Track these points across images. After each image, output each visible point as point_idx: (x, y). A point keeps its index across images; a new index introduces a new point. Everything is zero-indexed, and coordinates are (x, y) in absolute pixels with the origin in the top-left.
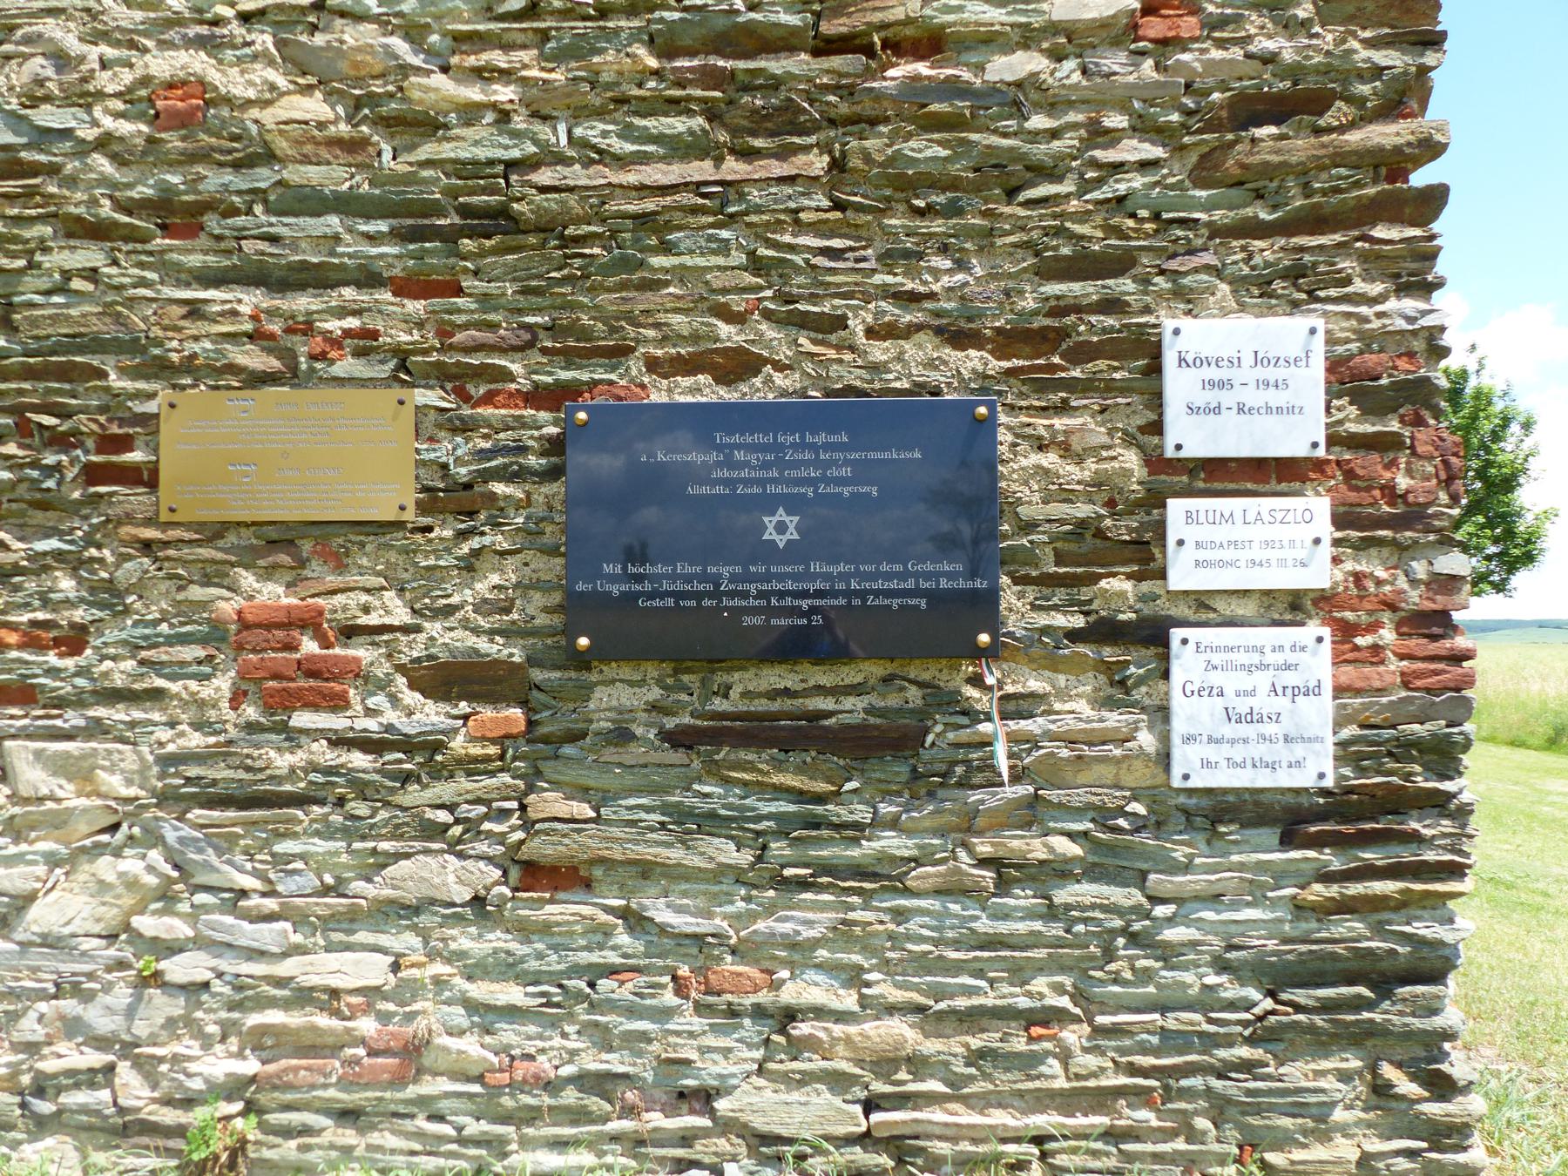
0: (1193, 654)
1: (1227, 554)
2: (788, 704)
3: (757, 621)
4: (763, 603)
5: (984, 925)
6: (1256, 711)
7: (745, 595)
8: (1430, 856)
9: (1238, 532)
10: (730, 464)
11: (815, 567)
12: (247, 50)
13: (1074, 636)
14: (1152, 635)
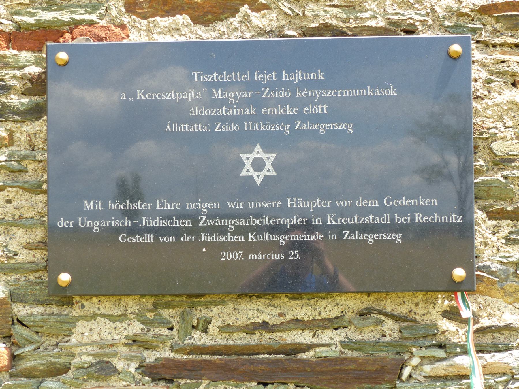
3: (235, 256)
7: (223, 231)
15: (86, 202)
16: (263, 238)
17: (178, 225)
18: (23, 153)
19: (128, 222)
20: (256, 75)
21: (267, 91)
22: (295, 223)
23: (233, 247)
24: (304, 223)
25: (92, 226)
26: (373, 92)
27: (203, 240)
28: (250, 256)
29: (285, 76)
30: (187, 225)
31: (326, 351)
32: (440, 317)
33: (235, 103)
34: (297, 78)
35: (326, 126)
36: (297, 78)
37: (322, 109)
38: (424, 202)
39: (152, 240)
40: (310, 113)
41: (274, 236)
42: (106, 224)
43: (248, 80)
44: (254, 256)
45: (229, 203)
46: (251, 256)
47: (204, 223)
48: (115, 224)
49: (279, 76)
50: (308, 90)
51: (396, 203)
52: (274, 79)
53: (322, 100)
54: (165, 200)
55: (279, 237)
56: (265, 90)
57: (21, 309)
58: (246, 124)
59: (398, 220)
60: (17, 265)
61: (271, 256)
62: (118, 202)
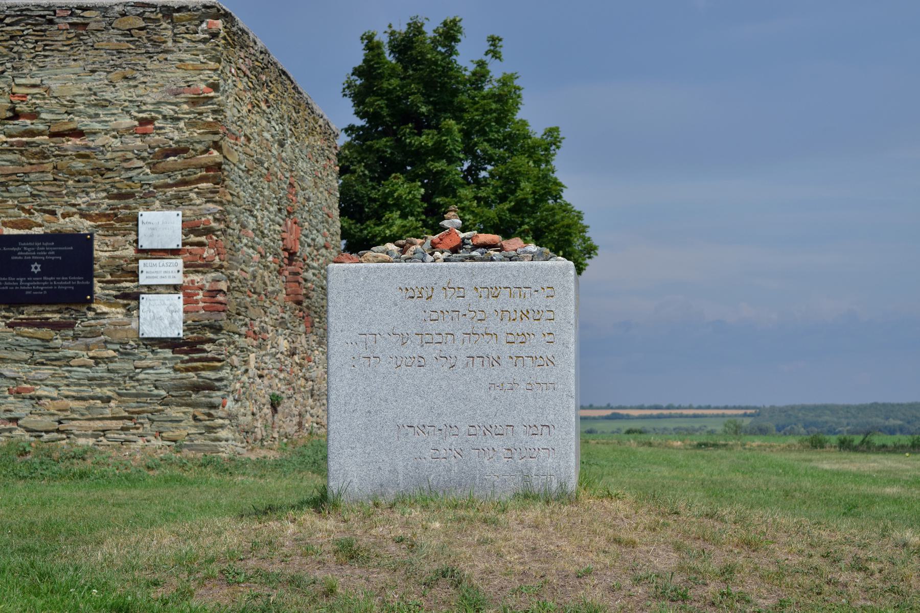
0: (148, 302)
1: (155, 275)
5: (91, 374)
6: (162, 316)
8: (210, 355)
9: (158, 269)
10: (23, 251)
11: (45, 278)
12: (462, 513)
13: (116, 297)
14: (136, 297)
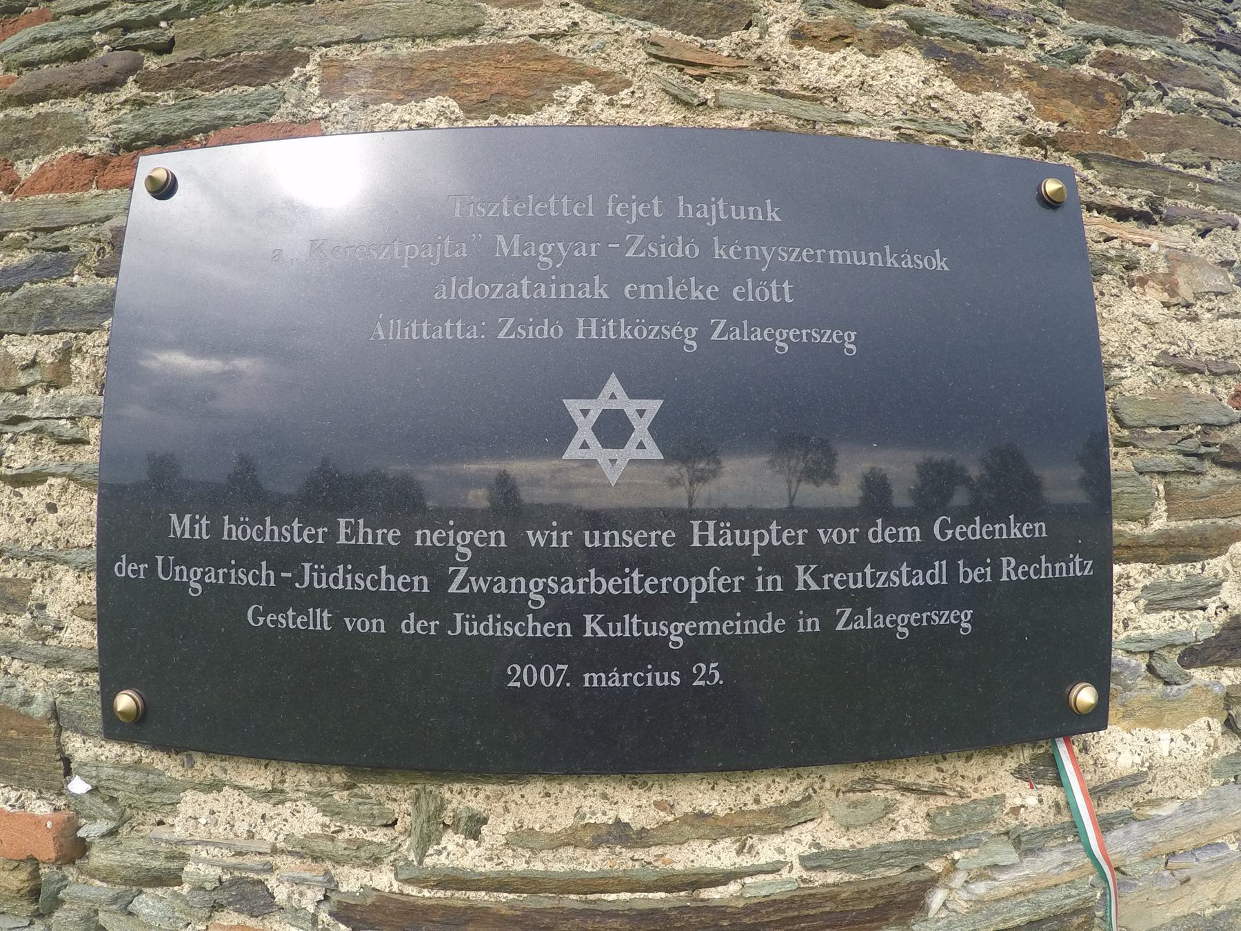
2: (625, 860)
3: (547, 676)
4: (565, 629)
7: (514, 608)
15: (174, 517)
16: (623, 631)
17: (392, 589)
18: (81, 400)
19: (268, 575)
20: (610, 205)
21: (638, 242)
22: (712, 590)
23: (541, 651)
24: (737, 590)
25: (185, 579)
26: (899, 260)
27: (459, 631)
28: (587, 676)
29: (684, 209)
30: (416, 589)
31: (770, 884)
32: (1012, 779)
33: (554, 271)
34: (714, 214)
35: (791, 333)
36: (714, 214)
37: (780, 292)
38: (1020, 530)
39: (326, 624)
40: (751, 299)
41: (654, 624)
42: (217, 577)
43: (590, 214)
44: (599, 678)
45: (530, 533)
46: (591, 679)
47: (461, 586)
48: (237, 578)
49: (669, 206)
50: (743, 245)
51: (963, 534)
52: (656, 214)
53: (779, 271)
54: (361, 521)
55: (668, 627)
56: (633, 240)
57: (78, 745)
58: (581, 321)
59: (966, 575)
60: (61, 651)
61: (645, 679)
62: (245, 522)
